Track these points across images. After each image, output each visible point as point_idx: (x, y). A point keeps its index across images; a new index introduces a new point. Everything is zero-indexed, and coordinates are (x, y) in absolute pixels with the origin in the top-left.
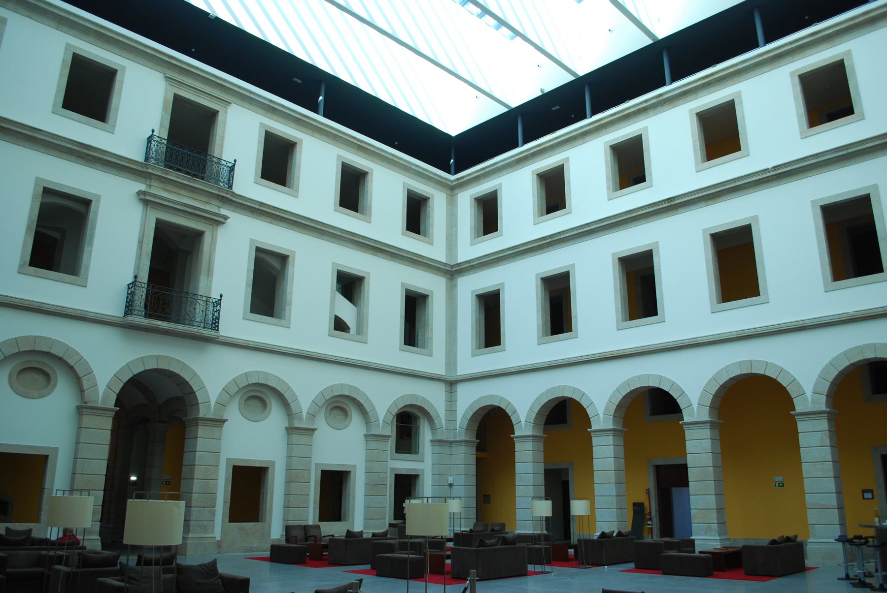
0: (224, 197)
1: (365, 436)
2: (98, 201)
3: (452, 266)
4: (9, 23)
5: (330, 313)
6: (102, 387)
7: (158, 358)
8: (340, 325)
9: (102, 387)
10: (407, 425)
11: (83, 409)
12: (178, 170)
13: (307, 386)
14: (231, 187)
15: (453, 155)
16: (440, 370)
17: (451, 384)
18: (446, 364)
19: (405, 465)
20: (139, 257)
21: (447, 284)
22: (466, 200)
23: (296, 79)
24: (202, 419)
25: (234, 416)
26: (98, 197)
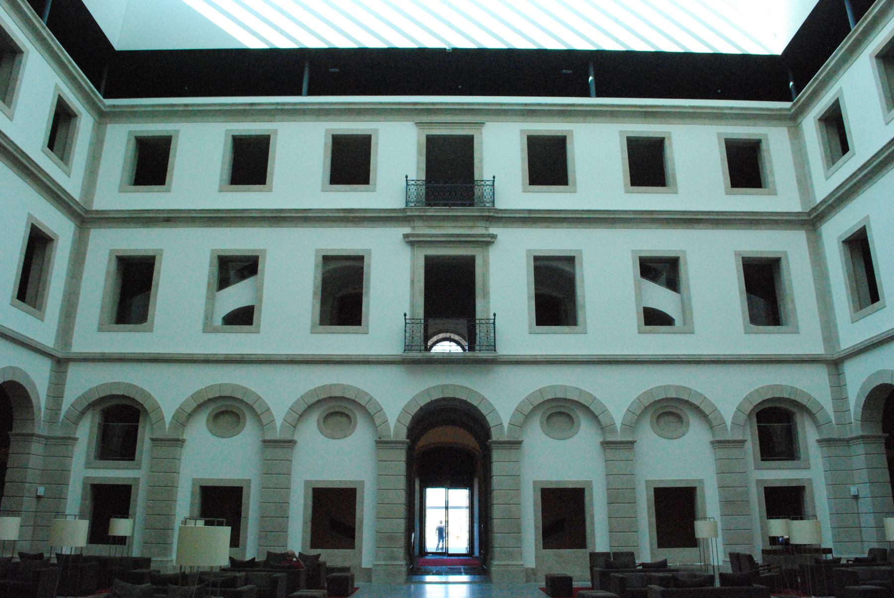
0: (489, 217)
1: (712, 443)
3: (809, 214)
4: (279, 132)
5: (637, 306)
6: (392, 422)
7: (443, 387)
8: (654, 318)
9: (392, 422)
10: (775, 425)
11: (382, 443)
12: (435, 205)
13: (618, 395)
14: (494, 206)
15: (591, 70)
16: (818, 349)
17: (835, 364)
18: (824, 340)
19: (781, 474)
20: (413, 296)
21: (808, 239)
23: (564, 71)
24: (495, 442)
25: (199, 433)
26: (369, 251)
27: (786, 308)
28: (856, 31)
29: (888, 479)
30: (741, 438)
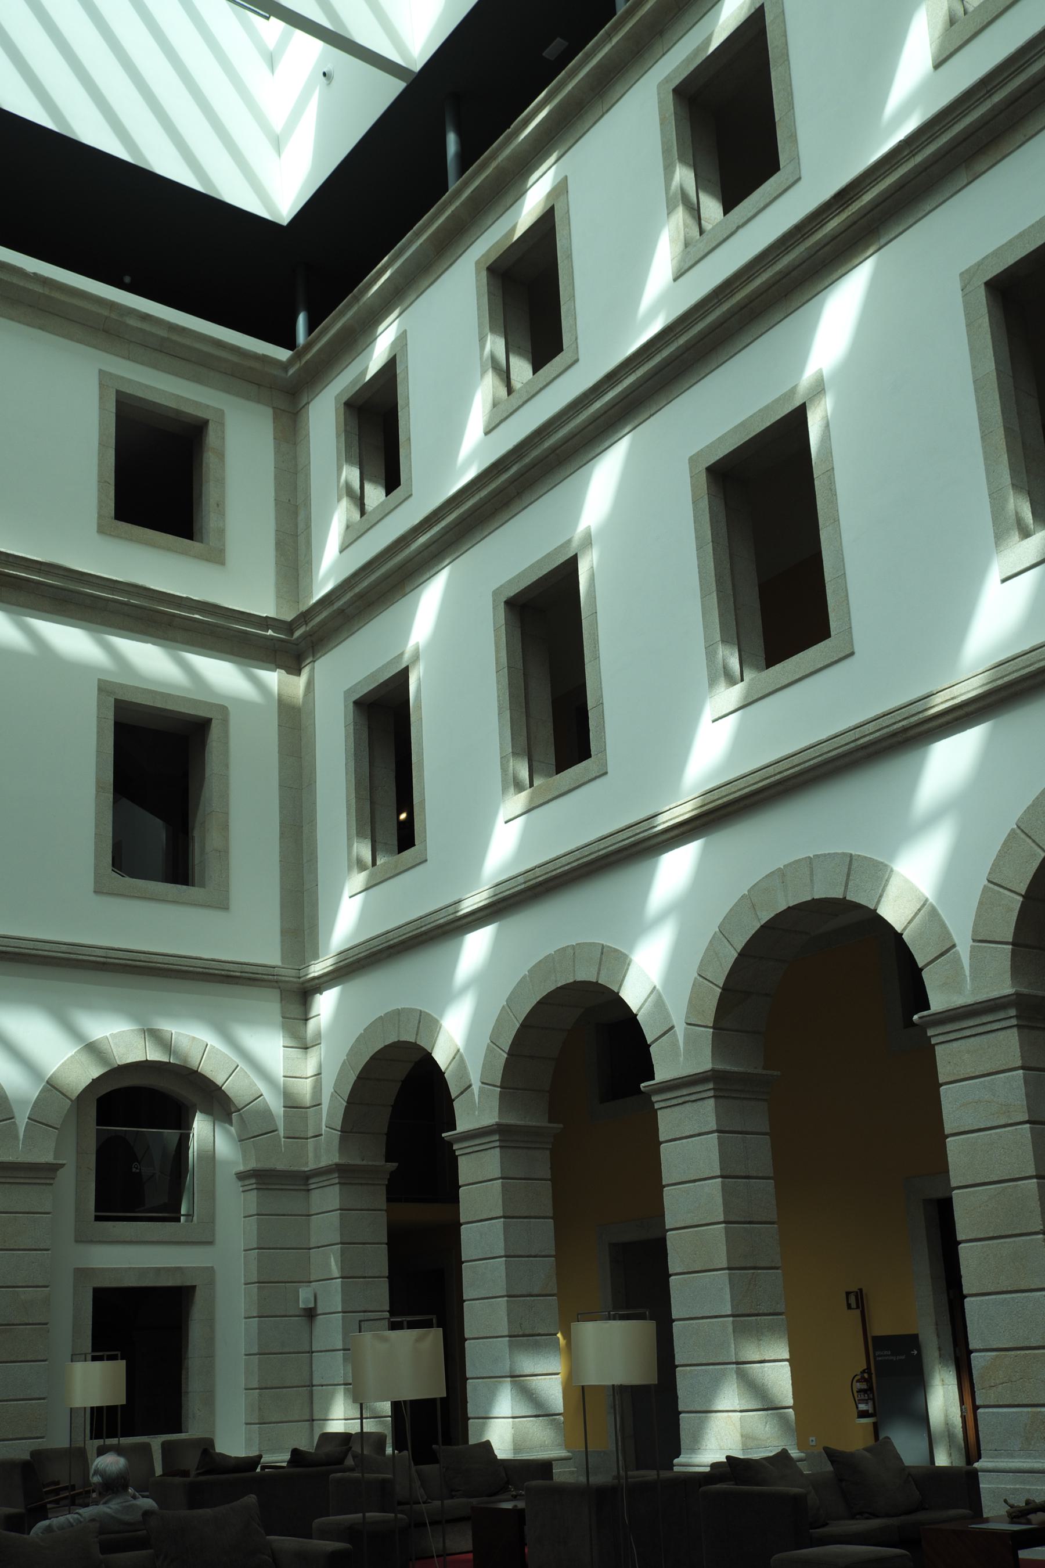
2: (211, 1284)
3: (289, 627)
16: (265, 951)
19: (135, 1255)
22: (324, 416)
27: (206, 839)
28: (459, 192)
29: (385, 1130)
30: (48, 1158)
